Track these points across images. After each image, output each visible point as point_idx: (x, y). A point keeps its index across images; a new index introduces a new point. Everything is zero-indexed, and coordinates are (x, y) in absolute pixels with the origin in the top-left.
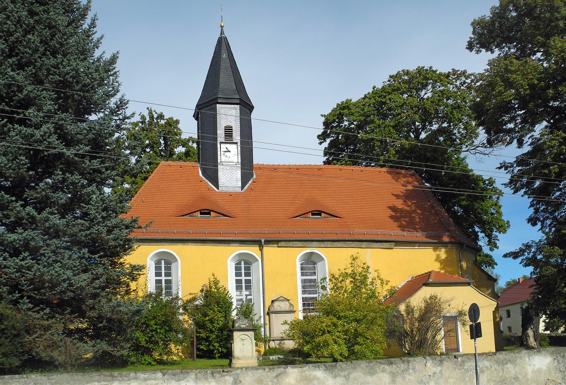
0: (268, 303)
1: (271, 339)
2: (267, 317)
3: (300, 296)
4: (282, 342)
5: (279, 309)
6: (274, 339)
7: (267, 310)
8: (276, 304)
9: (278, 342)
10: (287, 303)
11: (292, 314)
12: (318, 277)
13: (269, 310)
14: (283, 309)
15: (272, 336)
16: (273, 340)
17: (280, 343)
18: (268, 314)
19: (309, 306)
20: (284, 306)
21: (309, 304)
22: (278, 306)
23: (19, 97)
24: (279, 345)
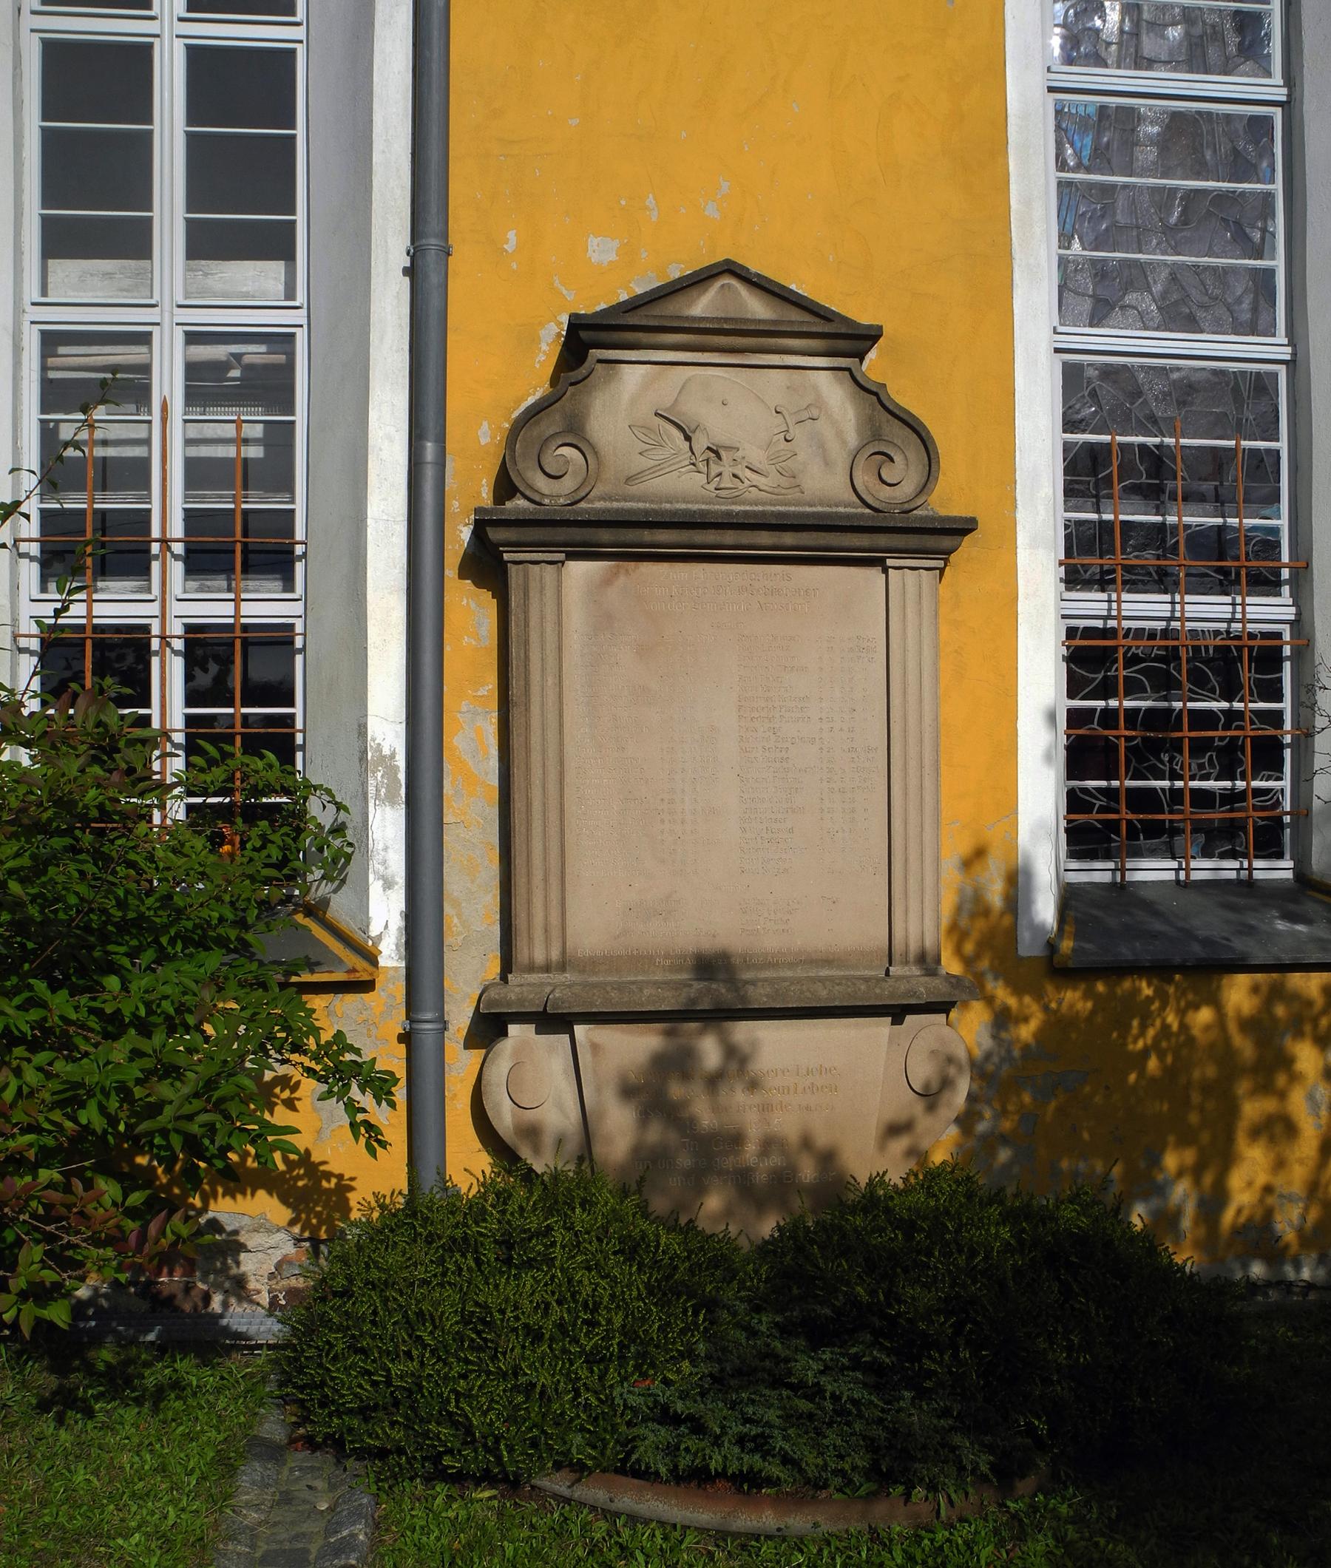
0: (500, 372)
1: (524, 990)
2: (471, 613)
3: (1036, 343)
4: (710, 1051)
5: (679, 484)
6: (560, 989)
7: (470, 488)
8: (631, 392)
9: (632, 1047)
10: (829, 389)
11: (909, 580)
12: (99, 1131)
13: (505, 486)
14: (757, 490)
15: (535, 949)
16: (553, 1021)
17: (674, 1063)
18: (486, 565)
19: (1153, 494)
20: (768, 429)
21: (1156, 460)
22: (645, 424)
23: (1186, 1196)
24: (650, 1093)
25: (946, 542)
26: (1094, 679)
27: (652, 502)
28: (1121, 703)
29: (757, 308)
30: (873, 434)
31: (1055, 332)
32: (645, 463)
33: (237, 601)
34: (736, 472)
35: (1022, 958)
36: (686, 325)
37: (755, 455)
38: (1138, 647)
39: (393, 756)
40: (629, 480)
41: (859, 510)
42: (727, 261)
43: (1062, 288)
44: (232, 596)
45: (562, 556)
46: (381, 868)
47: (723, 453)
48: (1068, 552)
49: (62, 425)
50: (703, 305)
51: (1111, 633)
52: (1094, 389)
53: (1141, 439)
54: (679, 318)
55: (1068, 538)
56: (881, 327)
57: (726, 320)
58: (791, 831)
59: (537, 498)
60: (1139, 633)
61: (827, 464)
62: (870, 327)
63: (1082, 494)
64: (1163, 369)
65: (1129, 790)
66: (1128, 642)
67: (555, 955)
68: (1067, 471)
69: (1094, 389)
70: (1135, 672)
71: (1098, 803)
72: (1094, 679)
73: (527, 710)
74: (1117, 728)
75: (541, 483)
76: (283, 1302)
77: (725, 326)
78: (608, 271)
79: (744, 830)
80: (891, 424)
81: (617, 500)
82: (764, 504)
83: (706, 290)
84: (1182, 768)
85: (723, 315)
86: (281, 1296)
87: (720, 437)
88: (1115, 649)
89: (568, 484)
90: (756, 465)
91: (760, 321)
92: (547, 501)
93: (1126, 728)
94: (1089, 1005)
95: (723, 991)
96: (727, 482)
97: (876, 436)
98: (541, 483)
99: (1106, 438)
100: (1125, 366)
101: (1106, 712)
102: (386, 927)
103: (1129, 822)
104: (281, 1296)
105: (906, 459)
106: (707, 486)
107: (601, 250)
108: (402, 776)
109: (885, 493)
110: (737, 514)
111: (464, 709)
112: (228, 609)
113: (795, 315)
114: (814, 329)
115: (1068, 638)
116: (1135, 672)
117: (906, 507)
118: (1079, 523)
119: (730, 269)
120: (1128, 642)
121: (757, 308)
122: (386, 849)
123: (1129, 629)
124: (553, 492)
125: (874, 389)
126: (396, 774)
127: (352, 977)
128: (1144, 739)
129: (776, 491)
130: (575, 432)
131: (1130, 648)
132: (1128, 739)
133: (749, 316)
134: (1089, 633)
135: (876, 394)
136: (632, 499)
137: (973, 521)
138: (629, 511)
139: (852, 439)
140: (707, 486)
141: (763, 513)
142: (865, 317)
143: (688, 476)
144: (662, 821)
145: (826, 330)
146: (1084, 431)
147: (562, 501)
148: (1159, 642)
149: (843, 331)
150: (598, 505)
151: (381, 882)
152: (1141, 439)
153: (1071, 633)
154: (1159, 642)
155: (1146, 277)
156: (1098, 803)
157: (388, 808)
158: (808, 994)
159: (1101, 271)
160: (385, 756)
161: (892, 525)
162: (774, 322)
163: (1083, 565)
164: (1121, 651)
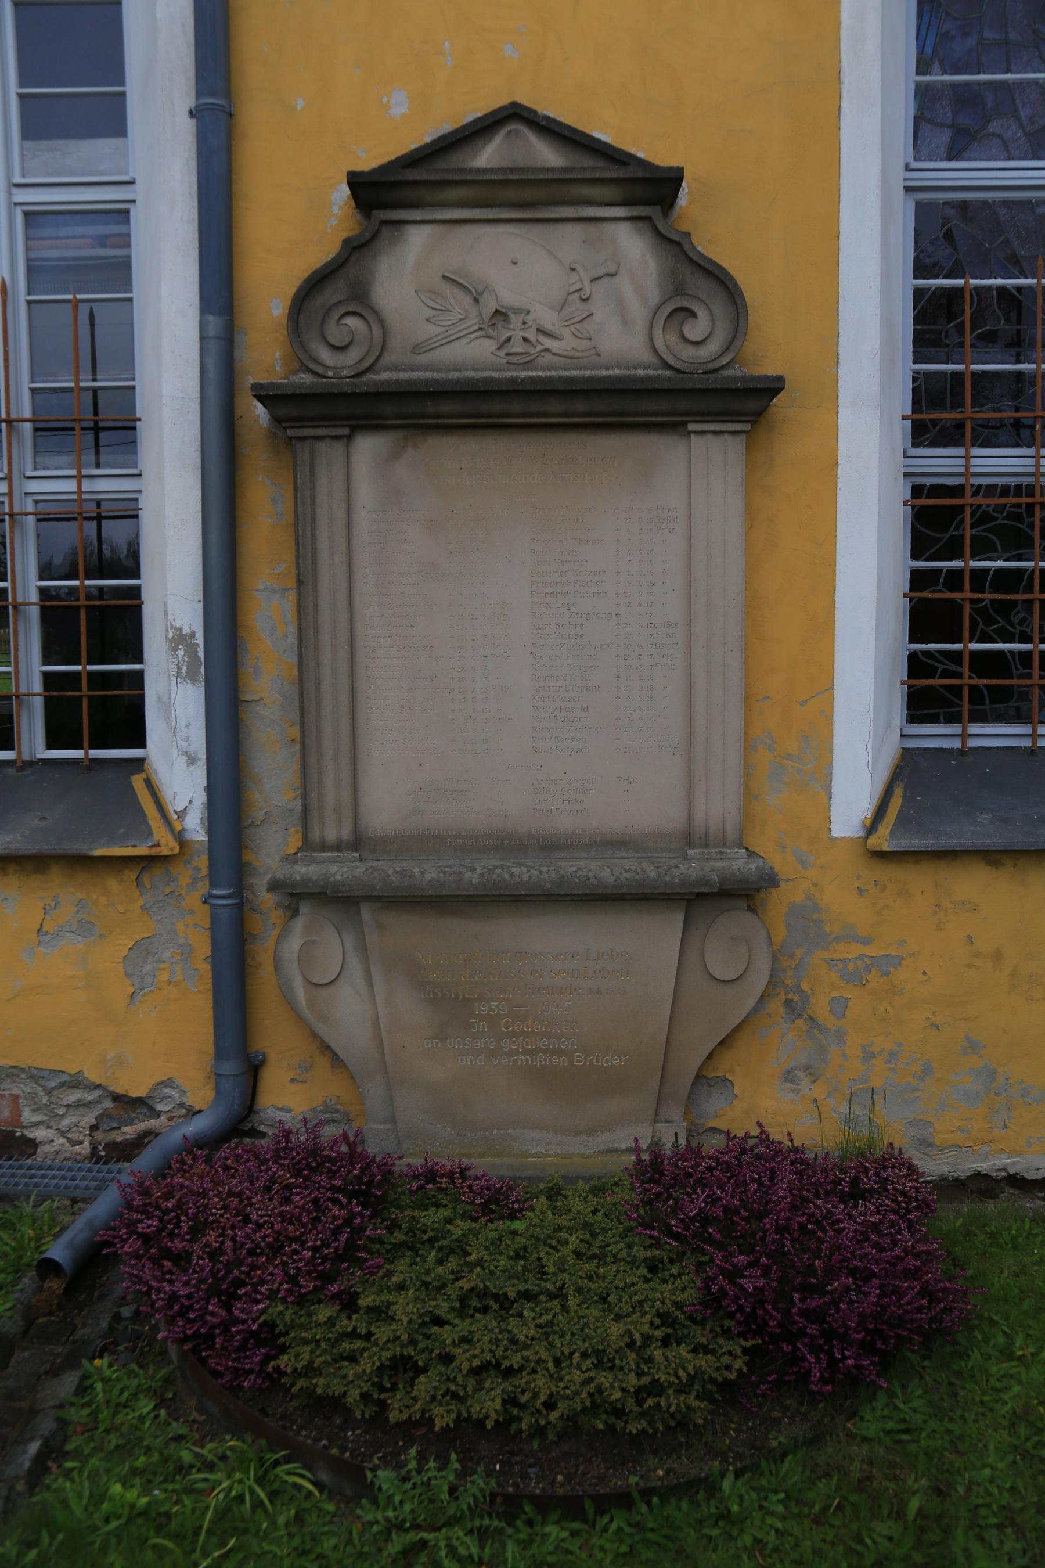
25: (752, 405)
26: (941, 539)
27: (439, 370)
28: (966, 564)
29: (547, 155)
30: (676, 288)
31: (908, 168)
32: (432, 330)
33: (80, 478)
34: (527, 335)
35: (834, 840)
36: (469, 178)
37: (548, 318)
38: (988, 505)
39: (193, 634)
40: (417, 349)
41: (660, 372)
42: (514, 105)
43: (917, 120)
44: (74, 472)
45: (346, 431)
46: (184, 744)
47: (512, 316)
48: (916, 402)
49: (80, 305)
50: (488, 156)
51: (957, 491)
52: (950, 230)
53: (1000, 282)
54: (462, 170)
55: (915, 391)
56: (680, 170)
57: (512, 170)
58: (586, 709)
59: (320, 370)
60: (991, 490)
61: (625, 323)
62: (670, 169)
63: (936, 343)
64: (1029, 202)
65: (974, 654)
66: (979, 500)
67: (346, 834)
68: (917, 320)
69: (950, 230)
70: (985, 530)
71: (941, 667)
72: (941, 539)
73: (315, 589)
74: (961, 590)
75: (326, 356)
76: (103, 1153)
77: (511, 177)
78: (397, 125)
79: (536, 709)
80: (697, 278)
81: (404, 370)
82: (556, 369)
83: (490, 140)
84: (1032, 631)
85: (510, 165)
86: (101, 1148)
87: (508, 298)
88: (961, 508)
89: (353, 356)
90: (548, 326)
91: (549, 170)
92: (330, 374)
93: (972, 590)
94: (283, 1381)
95: (516, 870)
96: (518, 347)
97: (679, 290)
98: (326, 356)
99: (959, 282)
100: (985, 203)
101: (951, 571)
102: (190, 802)
103: (973, 689)
104: (101, 1148)
105: (711, 314)
106: (498, 353)
107: (399, 105)
108: (201, 654)
109: (688, 353)
110: (523, 380)
111: (261, 587)
112: (71, 486)
113: (586, 161)
114: (608, 175)
115: (913, 497)
116: (985, 530)
117: (711, 366)
118: (928, 374)
119: (515, 115)
120: (979, 500)
121: (547, 155)
122: (188, 726)
123: (980, 486)
124: (337, 365)
125: (677, 239)
126: (197, 652)
127: (154, 852)
128: (992, 601)
129: (571, 354)
130: (359, 298)
131: (979, 506)
132: (972, 601)
133: (538, 165)
134: (937, 491)
135: (678, 244)
136: (419, 368)
137: (780, 379)
138: (409, 382)
139: (654, 295)
140: (498, 353)
141: (551, 379)
142: (662, 157)
143: (477, 342)
144: (453, 700)
145: (622, 175)
146: (936, 277)
147: (345, 372)
148: (1012, 500)
149: (640, 175)
150: (384, 376)
151: (185, 758)
152: (1000, 282)
153: (917, 491)
154: (1012, 500)
155: (1013, 100)
156: (941, 667)
157: (189, 686)
158: (595, 882)
159: (966, 98)
160: (185, 635)
161: (690, 386)
162: (565, 170)
163: (931, 420)
164: (968, 511)
